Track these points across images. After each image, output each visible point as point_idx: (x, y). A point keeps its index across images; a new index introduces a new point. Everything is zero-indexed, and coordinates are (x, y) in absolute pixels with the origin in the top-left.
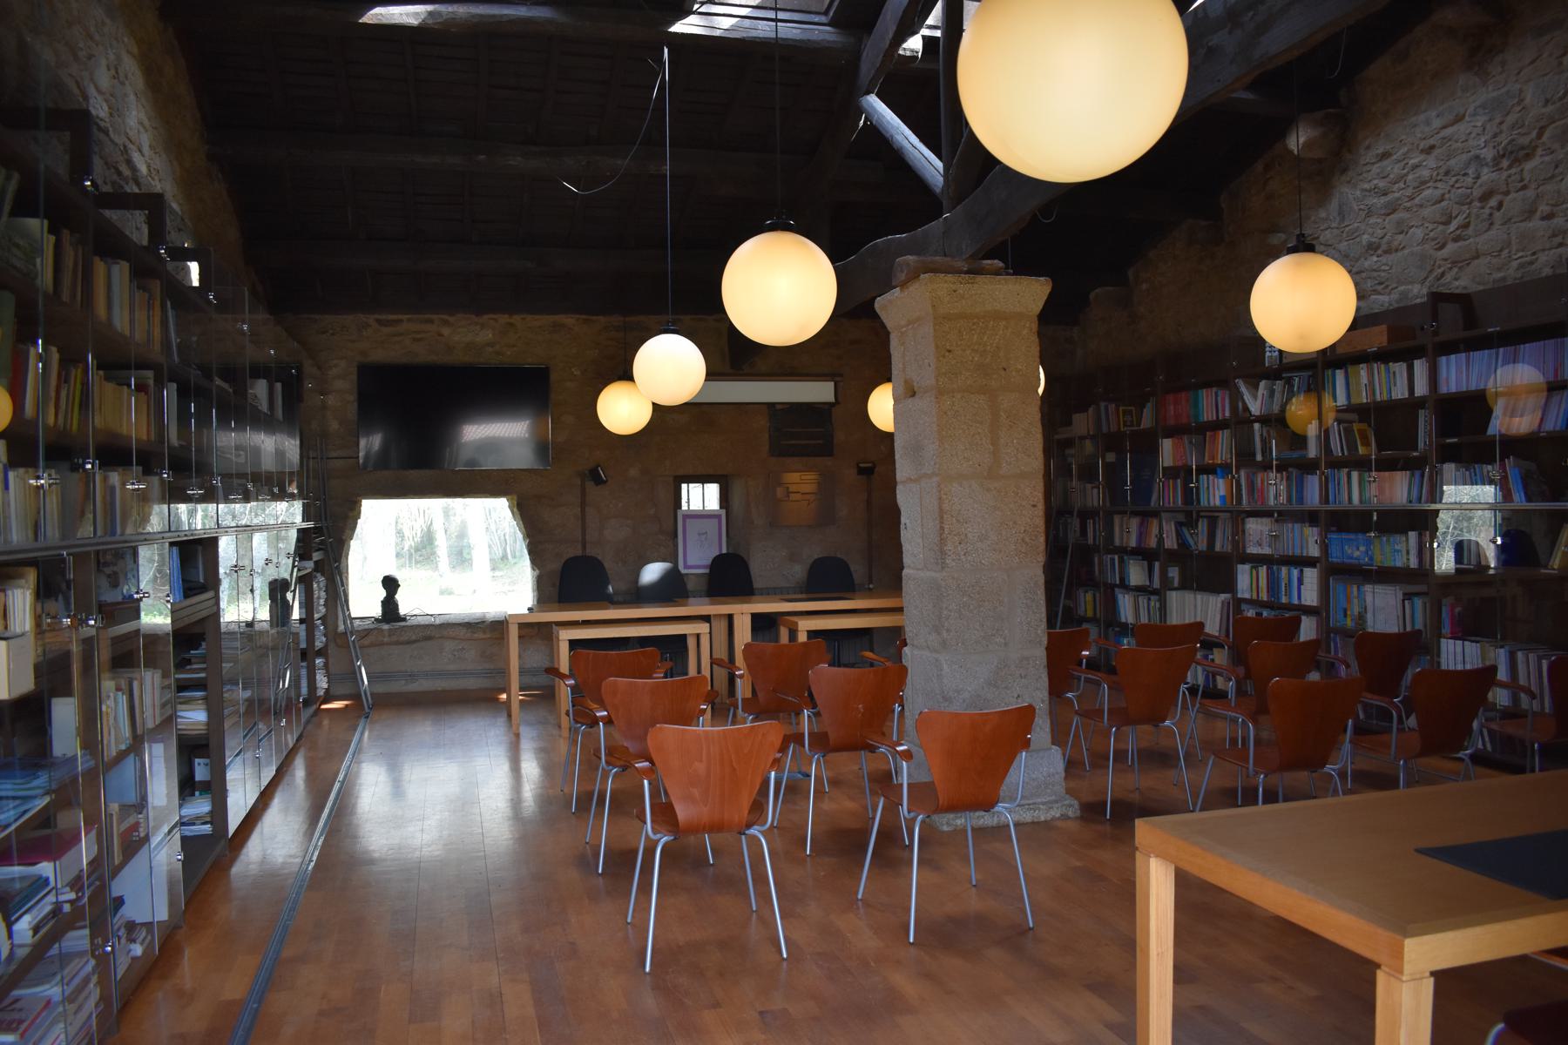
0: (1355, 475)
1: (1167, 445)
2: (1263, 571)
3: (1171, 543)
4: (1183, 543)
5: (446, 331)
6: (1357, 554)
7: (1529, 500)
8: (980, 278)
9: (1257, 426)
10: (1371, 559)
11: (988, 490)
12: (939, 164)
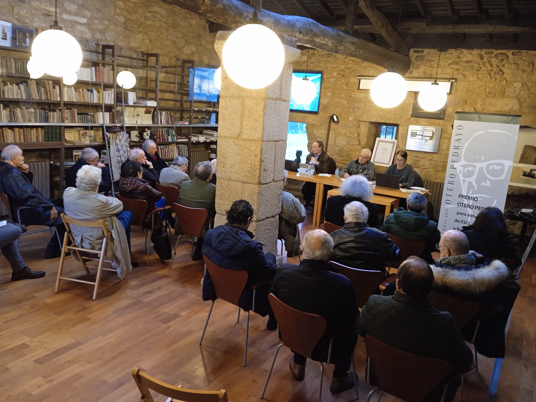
11: (237, 145)
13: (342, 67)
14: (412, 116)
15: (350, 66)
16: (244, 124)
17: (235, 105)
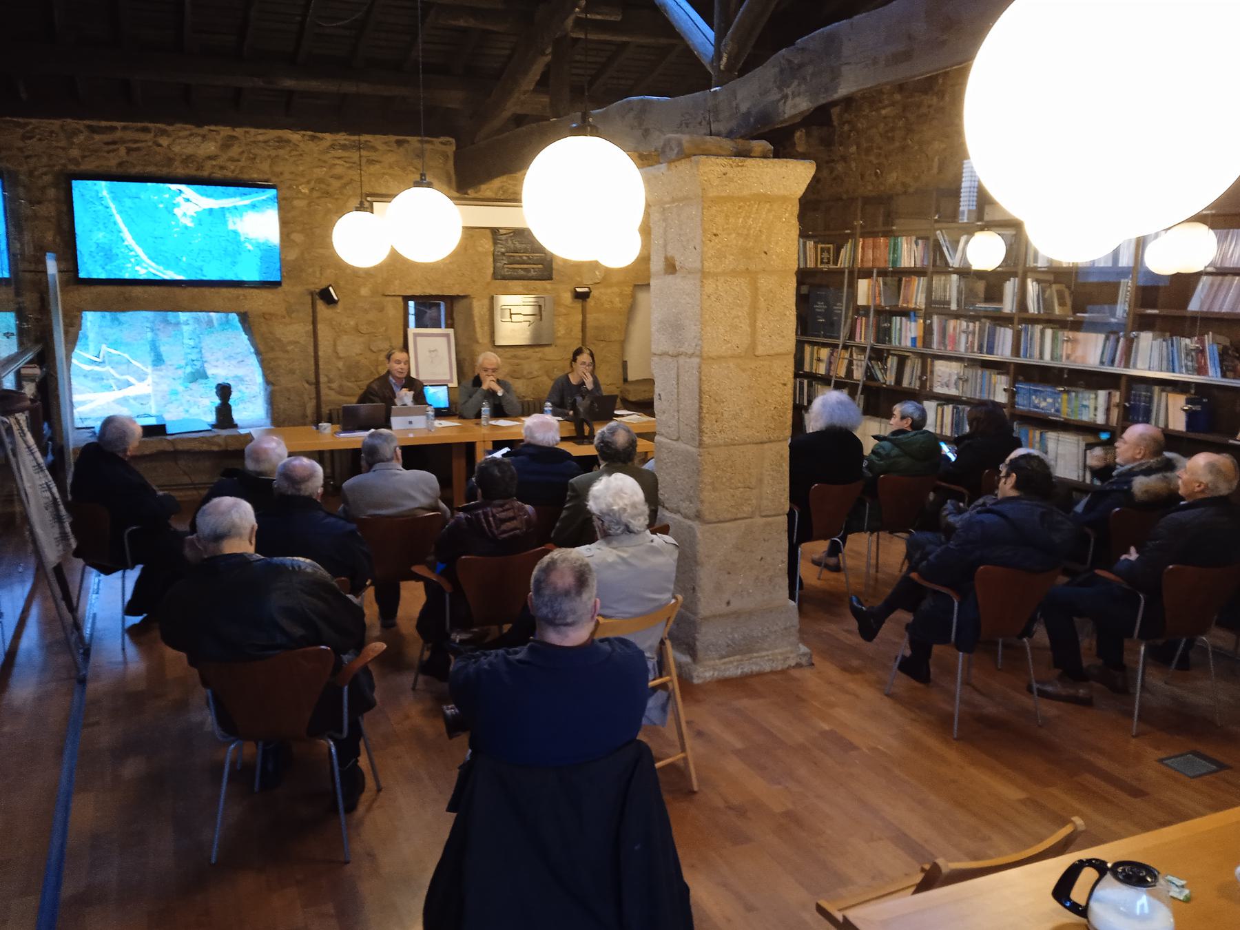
0: (1049, 332)
1: (863, 285)
2: (948, 409)
3: (858, 374)
4: (869, 374)
5: (164, 141)
6: (1043, 404)
7: (1224, 375)
8: (749, 161)
9: (955, 277)
10: (1057, 410)
11: (744, 370)
12: (711, 34)
13: (320, 172)
14: (495, 276)
15: (338, 170)
16: (759, 324)
17: (737, 289)
